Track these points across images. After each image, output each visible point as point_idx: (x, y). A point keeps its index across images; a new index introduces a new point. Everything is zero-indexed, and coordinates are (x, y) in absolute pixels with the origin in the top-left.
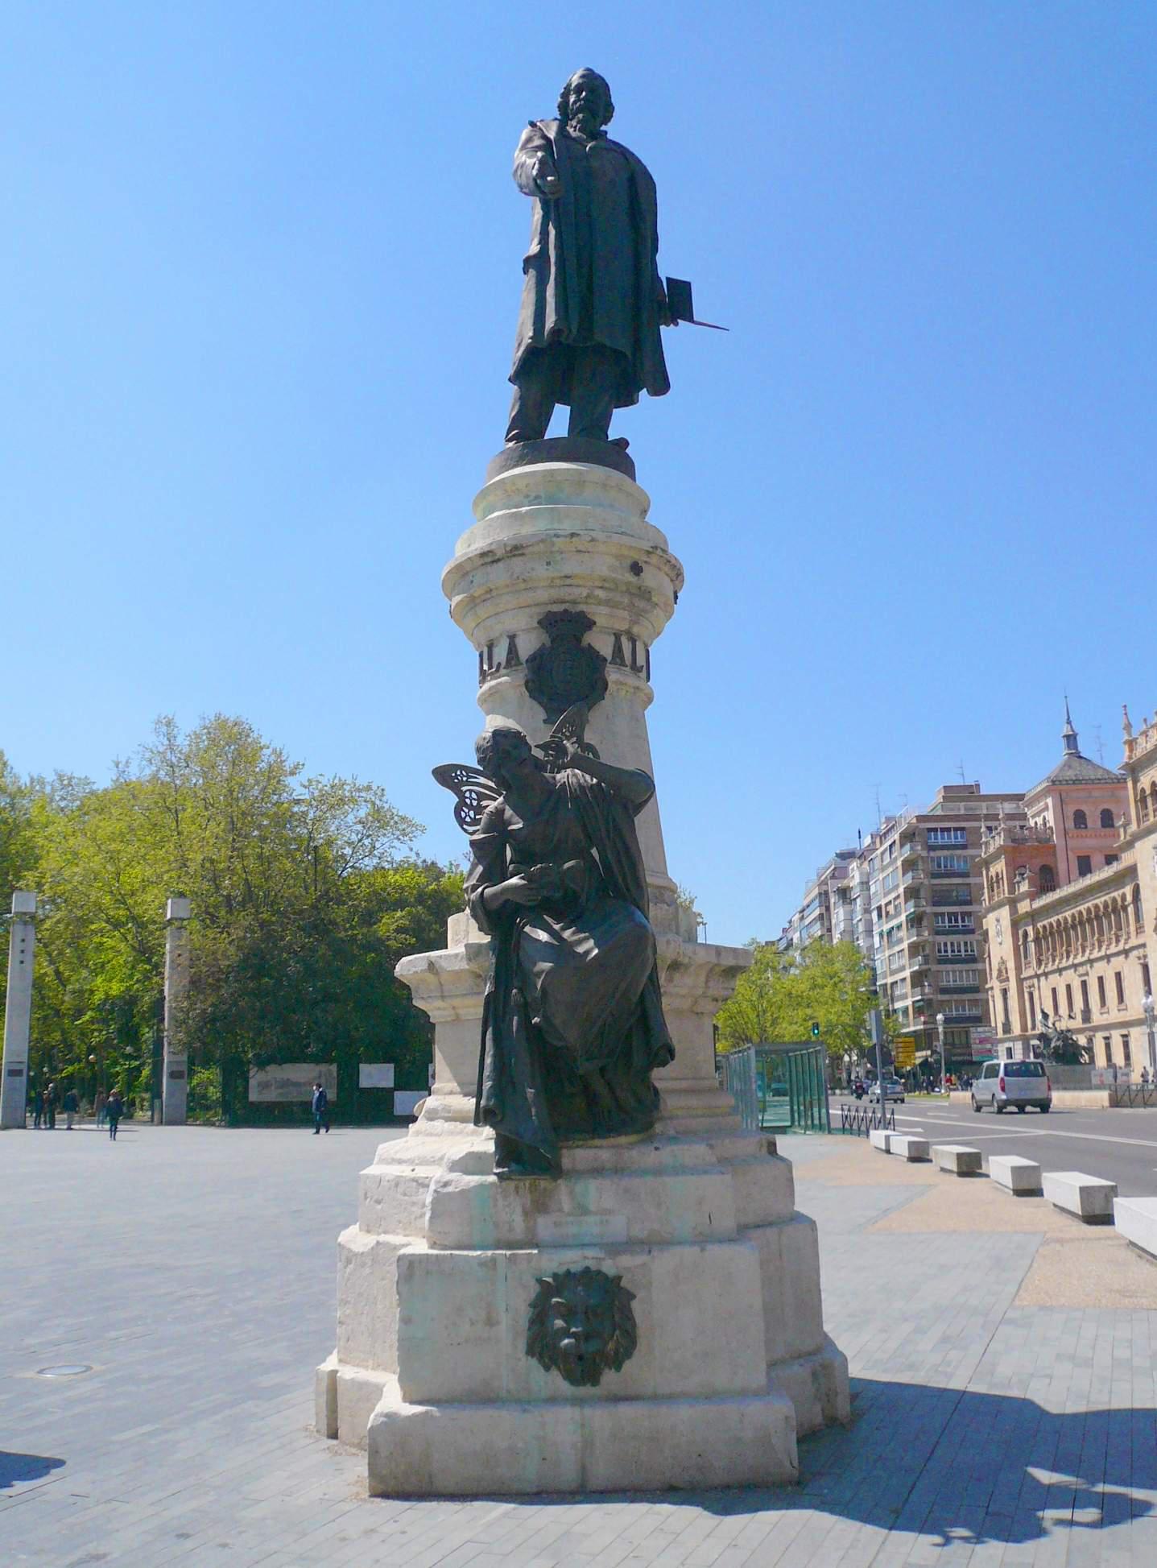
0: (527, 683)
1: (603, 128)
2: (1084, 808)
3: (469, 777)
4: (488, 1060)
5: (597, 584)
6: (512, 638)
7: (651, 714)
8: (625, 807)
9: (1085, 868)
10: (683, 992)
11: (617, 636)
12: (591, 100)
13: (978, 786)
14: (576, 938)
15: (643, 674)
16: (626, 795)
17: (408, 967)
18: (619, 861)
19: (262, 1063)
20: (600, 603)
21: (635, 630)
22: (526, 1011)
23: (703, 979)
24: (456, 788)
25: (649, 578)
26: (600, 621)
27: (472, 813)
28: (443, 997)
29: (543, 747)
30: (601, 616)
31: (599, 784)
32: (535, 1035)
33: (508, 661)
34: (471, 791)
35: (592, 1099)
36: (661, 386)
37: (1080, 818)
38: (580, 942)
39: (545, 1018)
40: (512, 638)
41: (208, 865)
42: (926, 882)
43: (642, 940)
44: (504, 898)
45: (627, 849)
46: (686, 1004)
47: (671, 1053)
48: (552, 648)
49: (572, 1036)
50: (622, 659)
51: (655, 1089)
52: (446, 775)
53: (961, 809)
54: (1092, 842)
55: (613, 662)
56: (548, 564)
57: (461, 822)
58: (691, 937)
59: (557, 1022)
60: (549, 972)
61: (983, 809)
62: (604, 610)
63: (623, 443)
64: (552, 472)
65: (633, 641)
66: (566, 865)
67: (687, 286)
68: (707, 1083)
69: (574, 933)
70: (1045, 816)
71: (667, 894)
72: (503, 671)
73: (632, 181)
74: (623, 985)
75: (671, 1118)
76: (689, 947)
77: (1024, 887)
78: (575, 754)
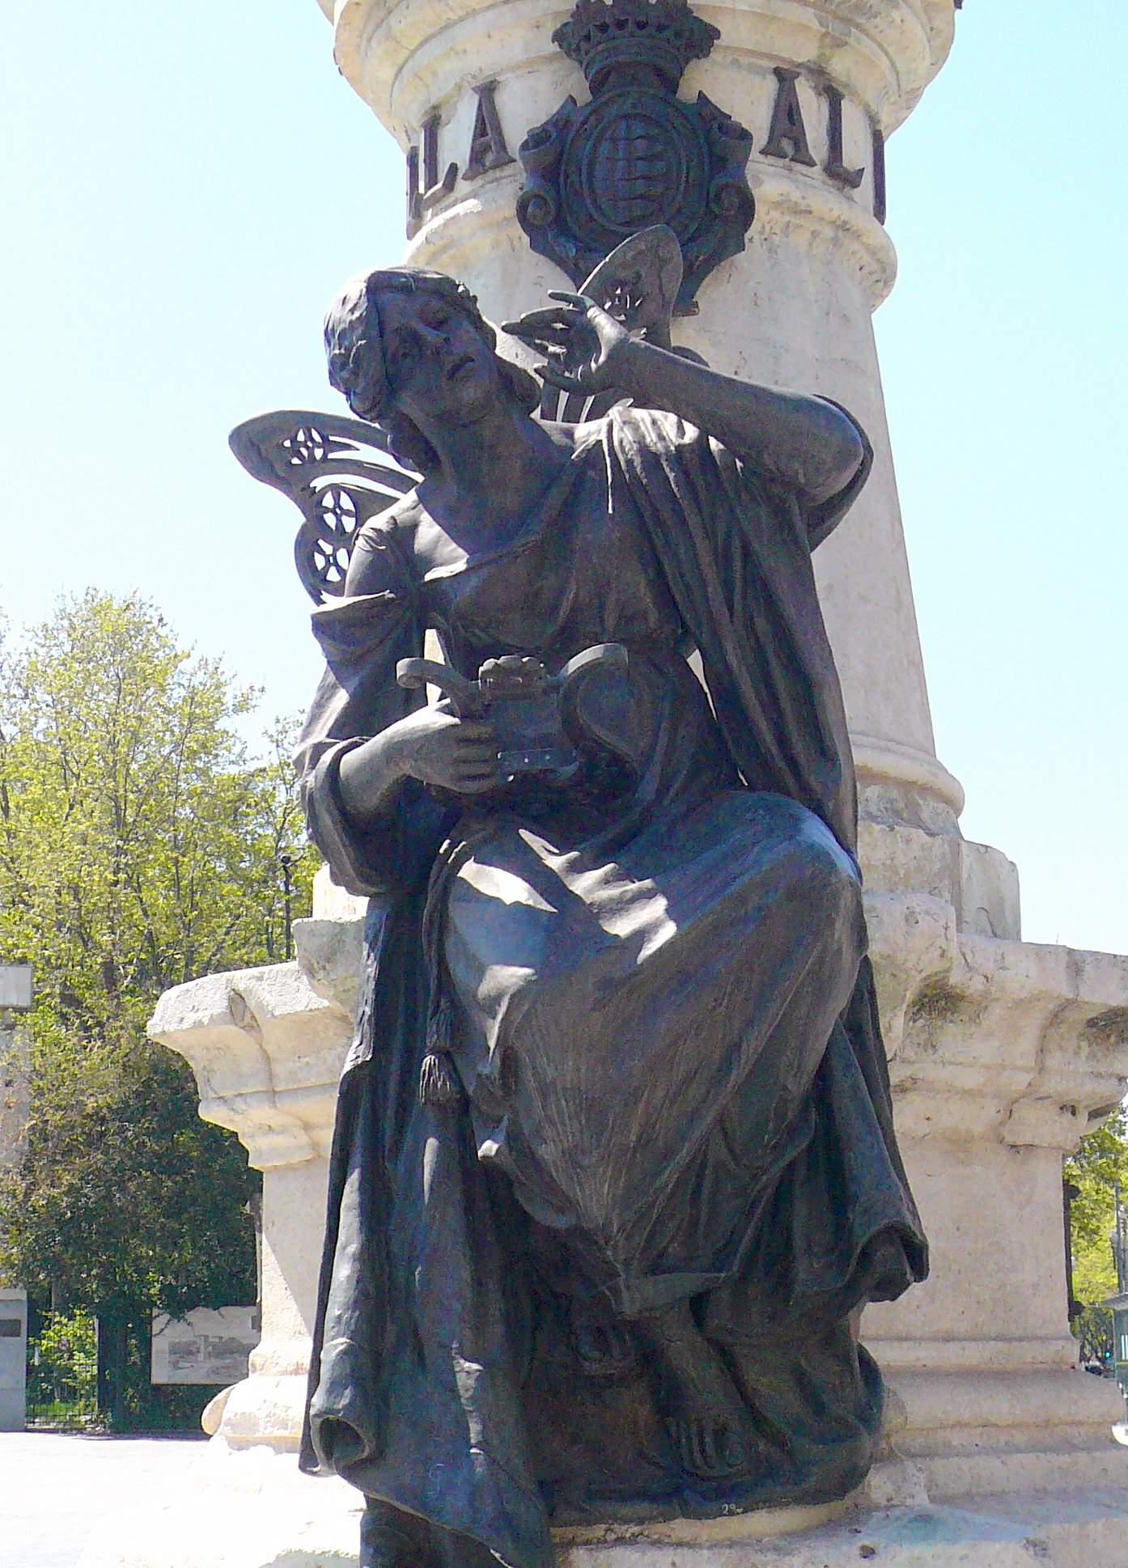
0: (522, 209)
3: (327, 444)
4: (343, 1271)
6: (488, 92)
7: (886, 320)
8: (780, 512)
10: (970, 1079)
11: (784, 77)
14: (613, 892)
15: (865, 190)
16: (791, 474)
18: (766, 678)
19: (178, 1306)
21: (840, 66)
22: (461, 1120)
23: (1027, 1044)
26: (733, 33)
28: (272, 1095)
29: (528, 330)
31: (701, 443)
32: (490, 1197)
33: (477, 157)
34: (336, 489)
35: (669, 1397)
38: (621, 906)
39: (514, 1141)
40: (488, 92)
41: (67, 898)
43: (819, 904)
44: (392, 775)
45: (782, 632)
46: (979, 1118)
47: (914, 1257)
48: (595, 110)
49: (597, 1197)
50: (799, 143)
51: (867, 1363)
52: (272, 448)
55: (771, 150)
58: (1001, 922)
59: (547, 1152)
60: (518, 996)
65: (833, 96)
66: (574, 664)
68: (1030, 1353)
69: (606, 882)
71: (928, 809)
72: (462, 186)
74: (753, 1046)
75: (928, 1454)
76: (985, 952)
78: (620, 349)
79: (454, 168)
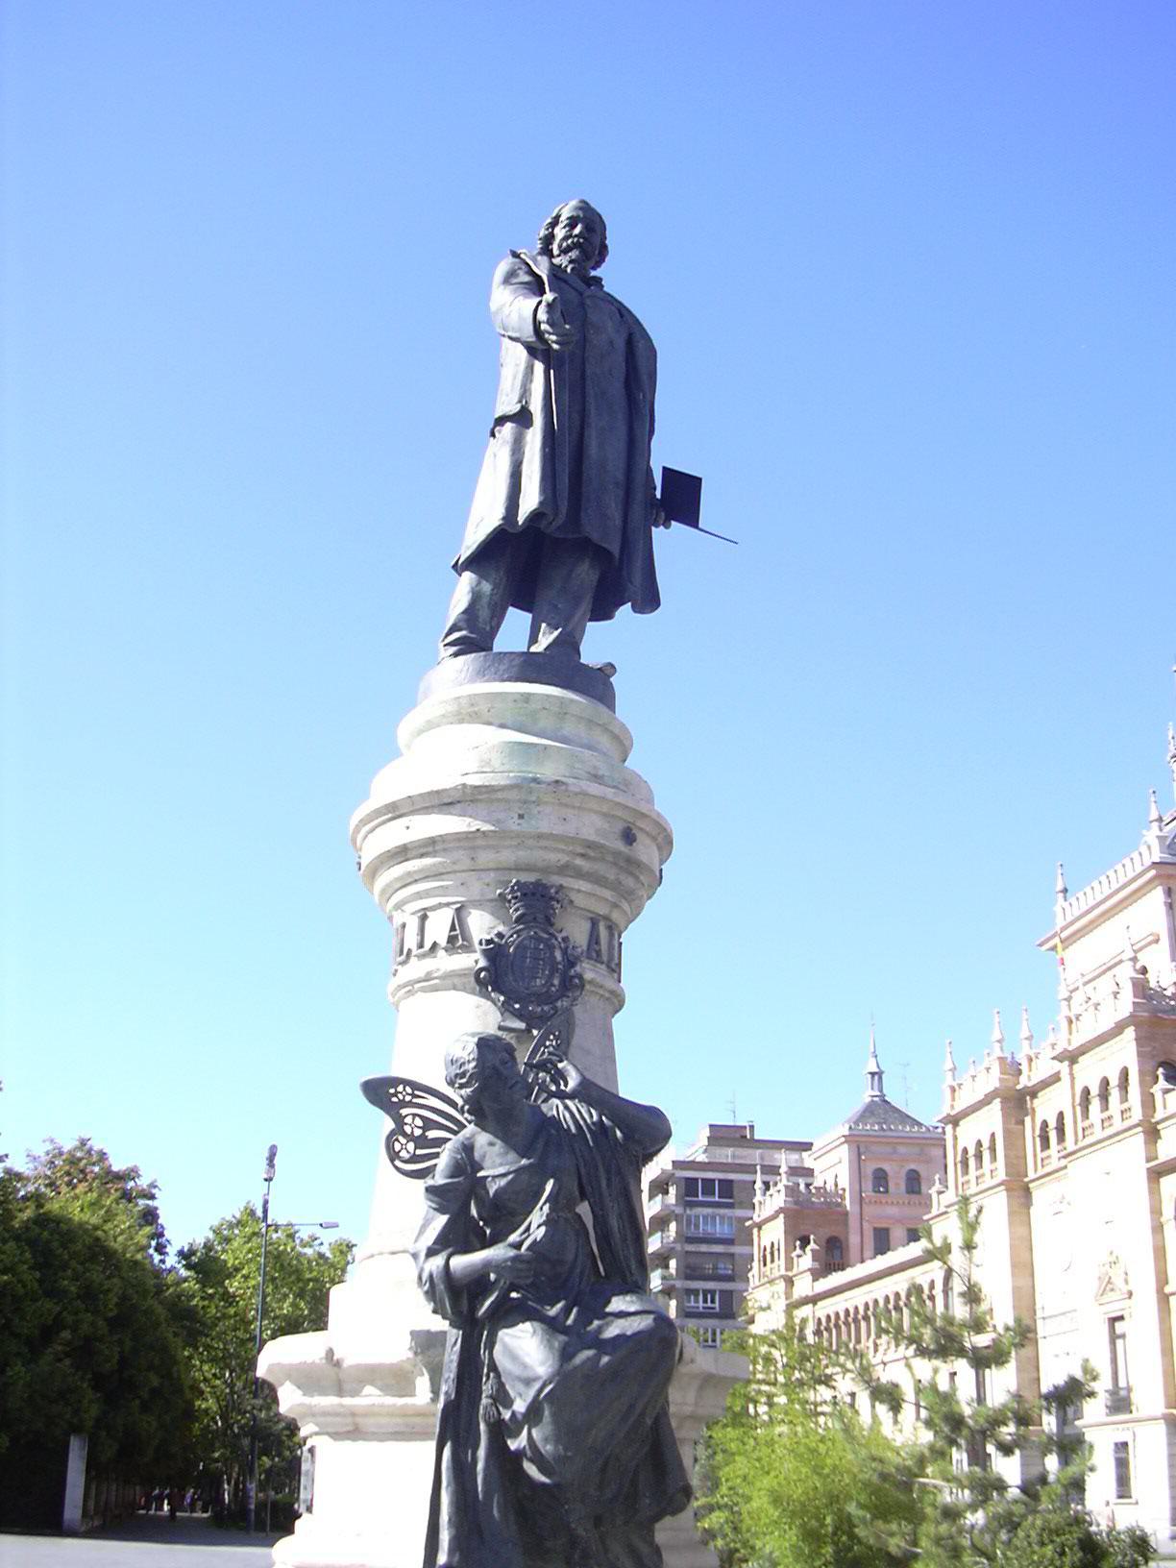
1: (593, 273)
2: (886, 1167)
5: (580, 850)
7: (618, 1022)
9: (882, 1245)
11: (594, 923)
12: (590, 236)
13: (752, 1127)
17: (276, 1356)
20: (579, 874)
24: (392, 1108)
25: (632, 852)
27: (411, 1146)
30: (580, 890)
33: (451, 940)
36: (649, 600)
37: (881, 1179)
42: (678, 1247)
50: (599, 953)
53: (726, 1155)
54: (892, 1211)
56: (521, 817)
57: (393, 1156)
61: (755, 1156)
62: (584, 886)
63: (606, 671)
64: (527, 698)
67: (695, 483)
70: (833, 1170)
72: (441, 953)
73: (630, 343)
77: (806, 1261)
79: (435, 945)
